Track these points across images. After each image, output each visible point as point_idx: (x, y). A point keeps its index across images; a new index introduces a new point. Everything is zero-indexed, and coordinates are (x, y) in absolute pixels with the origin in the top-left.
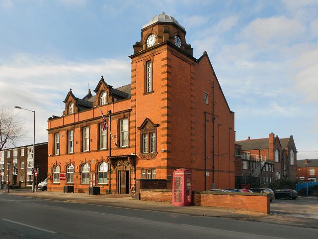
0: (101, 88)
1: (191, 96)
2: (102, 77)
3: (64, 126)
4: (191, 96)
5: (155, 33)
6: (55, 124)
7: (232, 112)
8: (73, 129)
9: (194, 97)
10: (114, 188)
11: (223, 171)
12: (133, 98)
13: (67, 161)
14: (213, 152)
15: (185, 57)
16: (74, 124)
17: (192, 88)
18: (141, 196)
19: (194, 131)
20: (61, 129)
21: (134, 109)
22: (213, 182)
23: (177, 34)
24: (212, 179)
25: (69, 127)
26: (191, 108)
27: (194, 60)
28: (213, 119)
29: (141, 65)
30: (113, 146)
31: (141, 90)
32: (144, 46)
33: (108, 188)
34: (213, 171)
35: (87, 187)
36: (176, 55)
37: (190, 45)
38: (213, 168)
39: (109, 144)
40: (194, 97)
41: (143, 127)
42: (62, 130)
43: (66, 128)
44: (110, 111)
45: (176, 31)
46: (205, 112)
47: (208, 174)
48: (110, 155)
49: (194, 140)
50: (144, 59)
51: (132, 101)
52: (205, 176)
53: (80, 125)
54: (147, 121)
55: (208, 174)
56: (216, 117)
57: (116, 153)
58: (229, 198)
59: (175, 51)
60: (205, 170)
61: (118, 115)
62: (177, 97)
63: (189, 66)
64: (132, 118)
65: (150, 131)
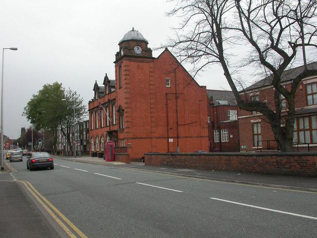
7: (202, 87)
14: (177, 123)
24: (176, 144)
28: (177, 98)
57: (112, 128)
59: (133, 58)
60: (168, 138)
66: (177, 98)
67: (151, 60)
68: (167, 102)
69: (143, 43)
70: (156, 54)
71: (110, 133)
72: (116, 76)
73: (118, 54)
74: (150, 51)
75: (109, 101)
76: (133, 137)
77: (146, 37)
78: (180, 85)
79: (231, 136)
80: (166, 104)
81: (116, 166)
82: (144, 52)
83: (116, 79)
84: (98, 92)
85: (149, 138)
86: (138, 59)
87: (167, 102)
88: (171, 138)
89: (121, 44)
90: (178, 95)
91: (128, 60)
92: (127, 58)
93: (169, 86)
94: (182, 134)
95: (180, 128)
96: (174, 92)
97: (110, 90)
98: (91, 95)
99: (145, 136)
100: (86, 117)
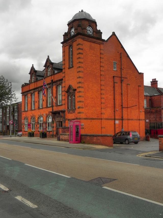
0: (48, 64)
1: (101, 66)
2: (33, 65)
3: (30, 91)
4: (101, 66)
5: (74, 27)
6: (26, 89)
7: (140, 73)
8: (34, 92)
9: (103, 67)
10: (55, 133)
11: (132, 120)
12: (64, 71)
13: (40, 114)
14: (122, 106)
15: (95, 40)
16: (34, 89)
17: (101, 61)
18: (60, 138)
19: (104, 91)
20: (28, 92)
21: (64, 78)
22: (122, 128)
23: (88, 25)
24: (121, 126)
25: (32, 91)
26: (101, 75)
27: (104, 40)
28: (121, 81)
29: (67, 47)
30: (54, 104)
31: (67, 66)
32: (69, 35)
33: (52, 133)
34: (122, 120)
35: (27, 133)
36: (87, 40)
37: (100, 30)
38: (122, 117)
39: (52, 104)
40: (103, 67)
41: (67, 92)
42: (29, 94)
43: (31, 92)
44: (52, 81)
45: (88, 23)
46: (114, 77)
47: (117, 122)
48: (53, 110)
49: (103, 98)
50: (68, 44)
51: (63, 73)
52: (115, 124)
53: (37, 89)
54: (70, 87)
55: (117, 122)
56: (124, 79)
57: (55, 109)
58: (95, 138)
59: (86, 38)
60: (115, 119)
61: (56, 83)
62: (88, 69)
63: (99, 45)
64: (63, 85)
65: (72, 94)
66: (121, 81)
67: (101, 42)
68: (114, 85)
69: (93, 23)
70: (105, 37)
71: (55, 114)
72: (64, 56)
73: (66, 35)
74: (100, 33)
75: (53, 82)
76: (85, 117)
77: (94, 16)
78: (124, 69)
79: (147, 121)
80: (114, 87)
81: (98, 150)
82: (95, 33)
83: (64, 60)
84: (36, 75)
85: (99, 119)
86: (91, 39)
87: (114, 85)
88: (117, 119)
89: (71, 24)
90: (122, 79)
91: (82, 38)
92: (81, 36)
93: (116, 70)
94: (125, 117)
95: (124, 110)
96: (120, 76)
97: (54, 72)
98: (26, 78)
99: (96, 117)
100: (18, 97)
